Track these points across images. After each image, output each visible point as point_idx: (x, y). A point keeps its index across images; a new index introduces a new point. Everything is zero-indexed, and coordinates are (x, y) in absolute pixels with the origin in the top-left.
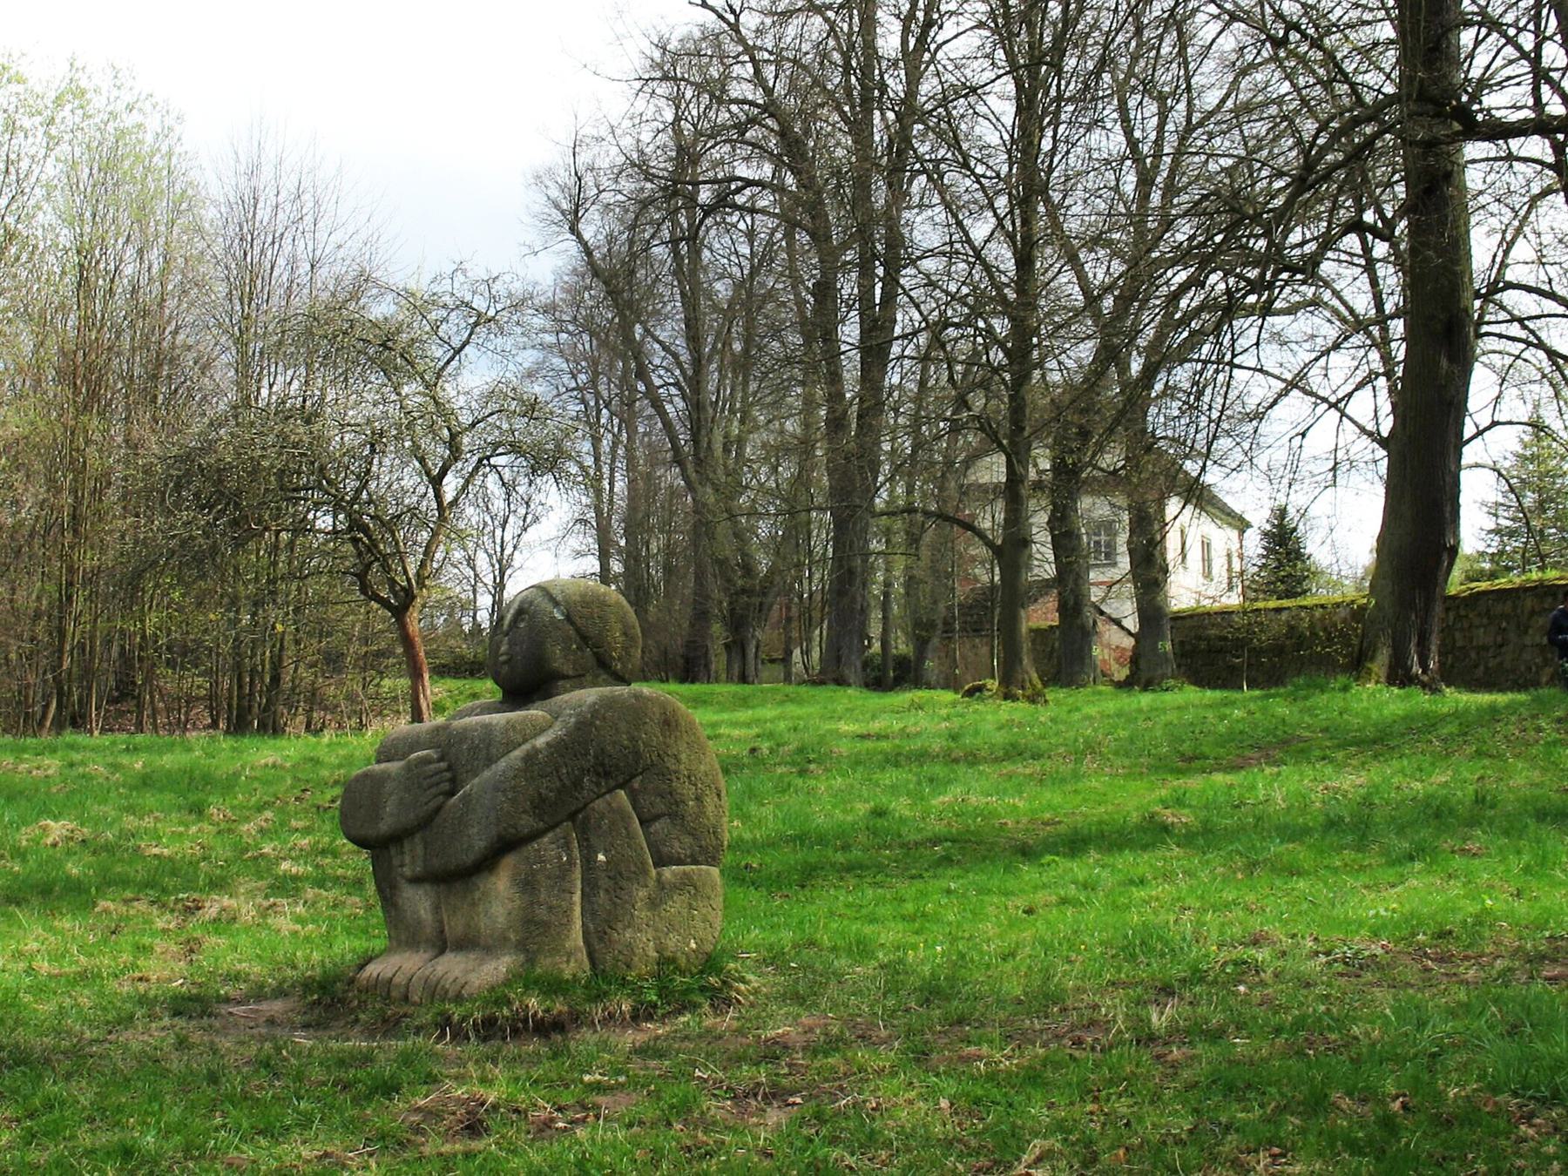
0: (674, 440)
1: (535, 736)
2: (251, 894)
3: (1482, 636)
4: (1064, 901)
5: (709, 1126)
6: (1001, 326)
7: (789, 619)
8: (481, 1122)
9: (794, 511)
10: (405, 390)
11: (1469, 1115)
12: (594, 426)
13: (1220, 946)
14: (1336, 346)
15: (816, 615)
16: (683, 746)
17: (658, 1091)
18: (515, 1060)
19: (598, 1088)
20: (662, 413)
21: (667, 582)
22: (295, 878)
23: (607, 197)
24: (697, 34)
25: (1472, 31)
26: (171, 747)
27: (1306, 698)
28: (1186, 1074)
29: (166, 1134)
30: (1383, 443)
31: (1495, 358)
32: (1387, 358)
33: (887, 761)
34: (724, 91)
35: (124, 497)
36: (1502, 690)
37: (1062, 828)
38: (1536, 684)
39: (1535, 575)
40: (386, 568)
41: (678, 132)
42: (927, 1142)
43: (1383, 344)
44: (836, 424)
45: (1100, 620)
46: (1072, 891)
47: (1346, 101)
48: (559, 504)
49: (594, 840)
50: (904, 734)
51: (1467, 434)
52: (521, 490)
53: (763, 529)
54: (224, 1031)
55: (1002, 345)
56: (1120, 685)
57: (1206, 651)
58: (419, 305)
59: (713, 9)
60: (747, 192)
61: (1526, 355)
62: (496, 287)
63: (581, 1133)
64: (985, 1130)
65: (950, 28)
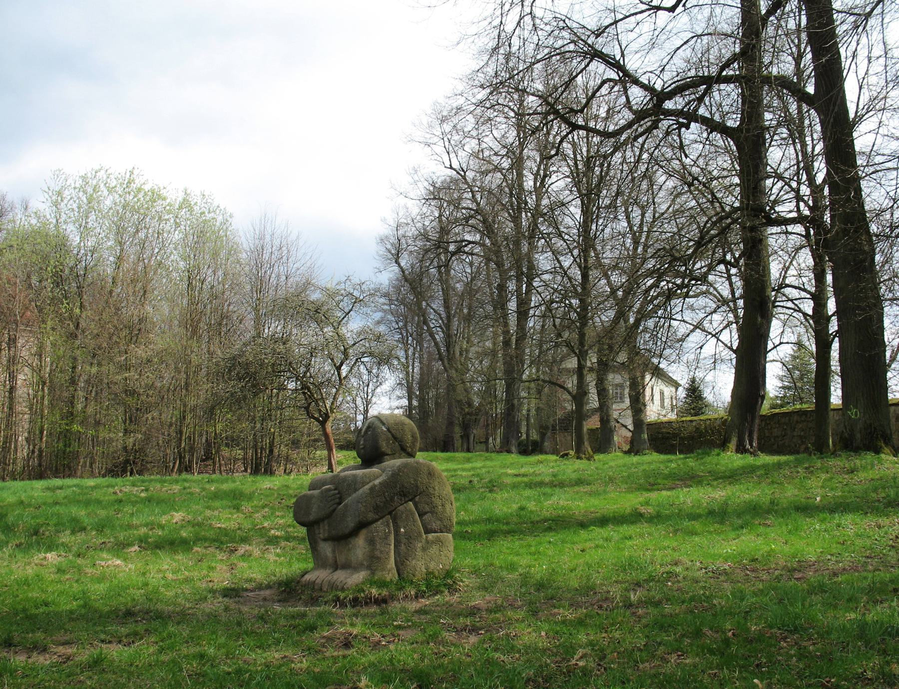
0: (439, 350)
1: (374, 480)
2: (258, 544)
3: (776, 432)
4: (597, 546)
5: (443, 643)
6: (575, 302)
7: (488, 425)
8: (350, 642)
9: (489, 381)
10: (325, 330)
11: (759, 638)
12: (406, 344)
13: (661, 565)
14: (715, 311)
15: (498, 423)
16: (436, 483)
17: (424, 629)
18: (366, 616)
19: (399, 627)
20: (434, 339)
21: (436, 410)
22: (277, 537)
23: (411, 248)
24: (448, 180)
25: (771, 180)
26: (226, 481)
27: (702, 458)
28: (644, 621)
29: (219, 648)
30: (735, 351)
31: (782, 316)
32: (736, 316)
33: (526, 486)
34: (459, 204)
35: (208, 374)
36: (784, 454)
37: (598, 515)
38: (798, 453)
39: (798, 407)
40: (317, 405)
41: (440, 221)
42: (536, 650)
43: (734, 311)
44: (507, 343)
45: (617, 425)
46: (601, 542)
47: (718, 209)
48: (390, 378)
49: (400, 524)
50: (534, 474)
51: (769, 348)
52: (374, 371)
53: (476, 387)
54: (244, 603)
55: (575, 311)
56: (625, 453)
57: (663, 438)
58: (331, 294)
59: (455, 170)
60: (470, 246)
61: (794, 314)
62: (364, 286)
63: (392, 647)
64: (559, 645)
65: (554, 178)
